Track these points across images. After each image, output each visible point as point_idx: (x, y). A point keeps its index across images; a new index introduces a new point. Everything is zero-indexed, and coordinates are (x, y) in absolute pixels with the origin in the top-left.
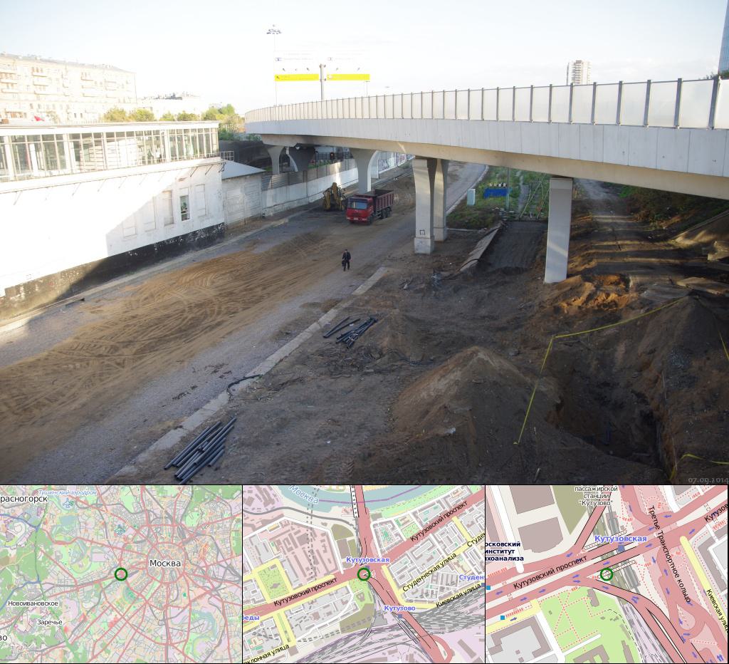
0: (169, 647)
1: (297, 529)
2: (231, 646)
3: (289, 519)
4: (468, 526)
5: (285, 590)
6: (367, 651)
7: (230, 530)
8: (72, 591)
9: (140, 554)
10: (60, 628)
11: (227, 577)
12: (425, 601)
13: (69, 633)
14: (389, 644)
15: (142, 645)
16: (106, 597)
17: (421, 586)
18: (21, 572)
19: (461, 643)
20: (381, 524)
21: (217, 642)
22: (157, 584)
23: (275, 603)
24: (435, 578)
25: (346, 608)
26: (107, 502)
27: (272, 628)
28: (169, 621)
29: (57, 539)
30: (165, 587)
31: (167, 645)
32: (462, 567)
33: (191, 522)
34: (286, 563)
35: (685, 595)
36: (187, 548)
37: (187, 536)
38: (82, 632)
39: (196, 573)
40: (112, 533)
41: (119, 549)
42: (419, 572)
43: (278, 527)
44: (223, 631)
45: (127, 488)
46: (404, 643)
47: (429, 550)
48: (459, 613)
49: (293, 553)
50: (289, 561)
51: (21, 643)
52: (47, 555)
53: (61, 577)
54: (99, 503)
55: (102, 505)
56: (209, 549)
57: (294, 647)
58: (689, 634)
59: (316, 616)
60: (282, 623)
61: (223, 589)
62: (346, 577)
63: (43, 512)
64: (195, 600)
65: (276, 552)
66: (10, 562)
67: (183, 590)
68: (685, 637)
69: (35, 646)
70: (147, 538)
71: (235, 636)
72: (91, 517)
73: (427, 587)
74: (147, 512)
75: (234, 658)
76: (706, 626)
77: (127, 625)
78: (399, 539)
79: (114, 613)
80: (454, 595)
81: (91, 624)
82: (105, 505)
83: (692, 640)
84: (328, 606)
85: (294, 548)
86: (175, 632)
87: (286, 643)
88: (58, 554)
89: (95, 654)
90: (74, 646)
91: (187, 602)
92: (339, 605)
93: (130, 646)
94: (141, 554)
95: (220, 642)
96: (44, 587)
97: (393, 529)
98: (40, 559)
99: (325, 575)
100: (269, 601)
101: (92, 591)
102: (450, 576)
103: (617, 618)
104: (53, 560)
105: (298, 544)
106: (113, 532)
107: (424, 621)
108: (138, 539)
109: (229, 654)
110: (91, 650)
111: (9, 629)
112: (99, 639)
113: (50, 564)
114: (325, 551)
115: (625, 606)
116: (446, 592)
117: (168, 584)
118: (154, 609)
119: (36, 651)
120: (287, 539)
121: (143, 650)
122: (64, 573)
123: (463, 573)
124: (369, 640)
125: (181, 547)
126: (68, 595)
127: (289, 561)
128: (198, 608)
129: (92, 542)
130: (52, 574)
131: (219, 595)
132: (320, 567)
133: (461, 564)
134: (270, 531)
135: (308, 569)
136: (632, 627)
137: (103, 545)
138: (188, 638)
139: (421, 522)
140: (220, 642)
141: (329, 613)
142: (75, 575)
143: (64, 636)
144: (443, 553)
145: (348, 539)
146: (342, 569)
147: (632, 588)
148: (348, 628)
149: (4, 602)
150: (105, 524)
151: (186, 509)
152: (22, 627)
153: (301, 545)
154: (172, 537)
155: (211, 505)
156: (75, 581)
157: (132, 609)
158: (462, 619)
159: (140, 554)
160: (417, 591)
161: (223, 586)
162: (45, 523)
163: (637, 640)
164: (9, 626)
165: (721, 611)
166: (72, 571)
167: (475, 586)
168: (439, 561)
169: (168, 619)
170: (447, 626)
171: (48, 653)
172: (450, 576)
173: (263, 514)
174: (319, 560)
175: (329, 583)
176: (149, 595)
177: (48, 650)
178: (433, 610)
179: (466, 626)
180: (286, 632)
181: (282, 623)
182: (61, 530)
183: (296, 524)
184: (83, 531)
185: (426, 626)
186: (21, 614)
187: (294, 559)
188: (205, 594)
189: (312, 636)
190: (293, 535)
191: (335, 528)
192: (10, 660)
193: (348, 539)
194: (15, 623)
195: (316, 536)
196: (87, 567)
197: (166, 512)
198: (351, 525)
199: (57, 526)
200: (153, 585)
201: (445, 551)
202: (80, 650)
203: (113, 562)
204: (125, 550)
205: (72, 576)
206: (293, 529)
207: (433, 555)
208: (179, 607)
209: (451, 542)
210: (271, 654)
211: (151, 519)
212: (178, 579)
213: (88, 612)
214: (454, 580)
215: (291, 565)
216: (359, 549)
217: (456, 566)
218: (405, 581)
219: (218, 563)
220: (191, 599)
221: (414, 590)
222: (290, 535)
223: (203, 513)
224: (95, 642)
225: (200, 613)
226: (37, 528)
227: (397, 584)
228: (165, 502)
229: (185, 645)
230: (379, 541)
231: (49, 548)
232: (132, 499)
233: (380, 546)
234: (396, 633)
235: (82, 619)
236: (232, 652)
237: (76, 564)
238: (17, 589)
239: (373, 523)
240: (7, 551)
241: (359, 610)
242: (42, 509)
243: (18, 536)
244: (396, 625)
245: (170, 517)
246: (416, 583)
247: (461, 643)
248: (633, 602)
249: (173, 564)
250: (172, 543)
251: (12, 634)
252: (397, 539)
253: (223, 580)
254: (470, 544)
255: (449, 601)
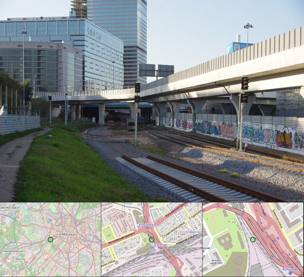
0: (70, 269)
1: (118, 212)
2: (96, 269)
3: (114, 208)
4: (190, 210)
5: (113, 237)
6: (148, 263)
7: (95, 221)
8: (29, 246)
9: (58, 231)
10: (25, 261)
11: (94, 240)
12: (172, 242)
13: (28, 264)
14: (157, 260)
15: (59, 268)
16: (43, 248)
17: (170, 236)
18: (8, 238)
19: (187, 259)
20: (153, 210)
21: (90, 267)
22: (65, 243)
23: (109, 243)
24: (176, 232)
25: (139, 245)
26: (44, 209)
27: (108, 253)
28: (70, 258)
29: (23, 224)
30: (68, 244)
31: (69, 269)
32: (187, 228)
33: (79, 217)
34: (114, 226)
35: (263, 212)
36: (77, 228)
37: (77, 223)
38: (33, 263)
39: (81, 239)
40: (46, 222)
41: (49, 228)
42: (169, 230)
43: (110, 211)
44: (93, 263)
45: (52, 203)
46: (163, 259)
47: (173, 220)
48: (186, 247)
49: (117, 222)
50: (115, 225)
51: (8, 268)
52: (19, 231)
53: (25, 240)
54: (40, 209)
55: (42, 210)
56: (86, 228)
57: (117, 261)
58: (265, 228)
59: (126, 248)
60: (112, 251)
61: (93, 245)
62: (140, 231)
63: (17, 213)
64: (81, 250)
65: (109, 221)
66: (4, 234)
67: (76, 246)
68: (263, 230)
69: (14, 269)
70: (61, 224)
71: (98, 265)
72: (37, 215)
73: (173, 236)
74: (61, 213)
75: (97, 274)
76: (272, 224)
77: (53, 260)
78: (161, 216)
79: (47, 255)
80: (184, 239)
81: (38, 259)
82: (43, 210)
83: (266, 231)
84: (131, 244)
85: (117, 219)
86: (72, 263)
87: (113, 259)
88: (24, 230)
89: (39, 272)
90: (30, 269)
91: (78, 251)
92: (136, 243)
93: (54, 269)
94: (58, 231)
95: (91, 267)
96: (18, 244)
97: (158, 212)
98: (16, 233)
99: (130, 231)
100: (107, 242)
101: (37, 246)
102: (182, 232)
103: (235, 222)
104: (21, 233)
105: (119, 218)
106: (46, 221)
107: (171, 250)
108: (57, 224)
109: (95, 272)
110: (37, 270)
111: (3, 262)
112: (41, 266)
113: (20, 235)
114: (130, 221)
115: (238, 217)
116: (180, 238)
117: (69, 243)
118: (64, 253)
119: (14, 271)
120: (114, 216)
121: (59, 270)
122: (26, 238)
123: (187, 230)
124: (148, 258)
125: (75, 228)
126: (28, 248)
127: (115, 225)
128: (82, 253)
129: (38, 225)
130: (21, 239)
131: (91, 248)
132: (128, 227)
133: (186, 226)
134: (107, 212)
135: (123, 228)
136: (241, 225)
137: (42, 227)
138: (78, 265)
139: (170, 209)
140: (91, 267)
141: (132, 247)
142: (31, 239)
143: (26, 265)
144: (179, 222)
145: (140, 216)
146: (137, 229)
147: (241, 209)
148: (140, 253)
149: (1, 250)
150: (43, 218)
151: (77, 212)
152: (8, 261)
153: (120, 218)
154: (71, 223)
155: (88, 210)
156: (31, 242)
157: (55, 254)
158: (187, 249)
159: (58, 231)
160: (168, 237)
161: (92, 244)
162: (18, 218)
163: (243, 230)
164: (3, 261)
165: (279, 219)
166: (29, 238)
167: (192, 235)
168: (177, 225)
169: (69, 258)
170: (181, 252)
171: (19, 272)
172: (182, 232)
173: (104, 205)
174: (128, 225)
175: (132, 234)
176: (62, 248)
177: (20, 270)
178: (175, 246)
179: (188, 252)
180: (114, 255)
181: (112, 251)
182: (25, 221)
183: (118, 210)
184: (34, 221)
185: (172, 252)
186: (8, 256)
187: (117, 224)
188: (85, 247)
189: (125, 257)
190: (117, 214)
191: (134, 211)
192: (3, 275)
193: (140, 216)
194: (6, 259)
195: (126, 215)
196: (36, 236)
197: (69, 213)
198: (141, 210)
199: (23, 219)
200: (63, 243)
201: (180, 221)
202: (33, 271)
203: (46, 234)
204: (51, 229)
205: (29, 240)
206: (117, 212)
207: (175, 223)
208: (74, 253)
209: (183, 217)
210: (108, 264)
211: (63, 216)
212: (74, 241)
213: (36, 255)
214: (184, 233)
215: (116, 227)
216: (144, 220)
217: (184, 227)
218: (163, 234)
219: (91, 234)
220: (79, 249)
221: (167, 237)
222: (115, 214)
223: (84, 214)
224: (39, 267)
225: (83, 255)
226: (15, 220)
227: (160, 235)
228: (68, 209)
229: (77, 268)
230: (152, 217)
231: (20, 228)
232: (55, 208)
233: (153, 219)
234: (159, 255)
235: (34, 258)
236: (96, 272)
237: (31, 235)
238: (7, 245)
239: (150, 209)
240: (2, 229)
241: (144, 246)
242: (17, 212)
243: (7, 223)
244: (159, 252)
245: (70, 215)
246: (168, 234)
247: (187, 259)
248: (242, 215)
249: (72, 235)
250: (71, 226)
251: (4, 264)
252: (160, 216)
253: (92, 242)
254: (190, 218)
255: (182, 242)
